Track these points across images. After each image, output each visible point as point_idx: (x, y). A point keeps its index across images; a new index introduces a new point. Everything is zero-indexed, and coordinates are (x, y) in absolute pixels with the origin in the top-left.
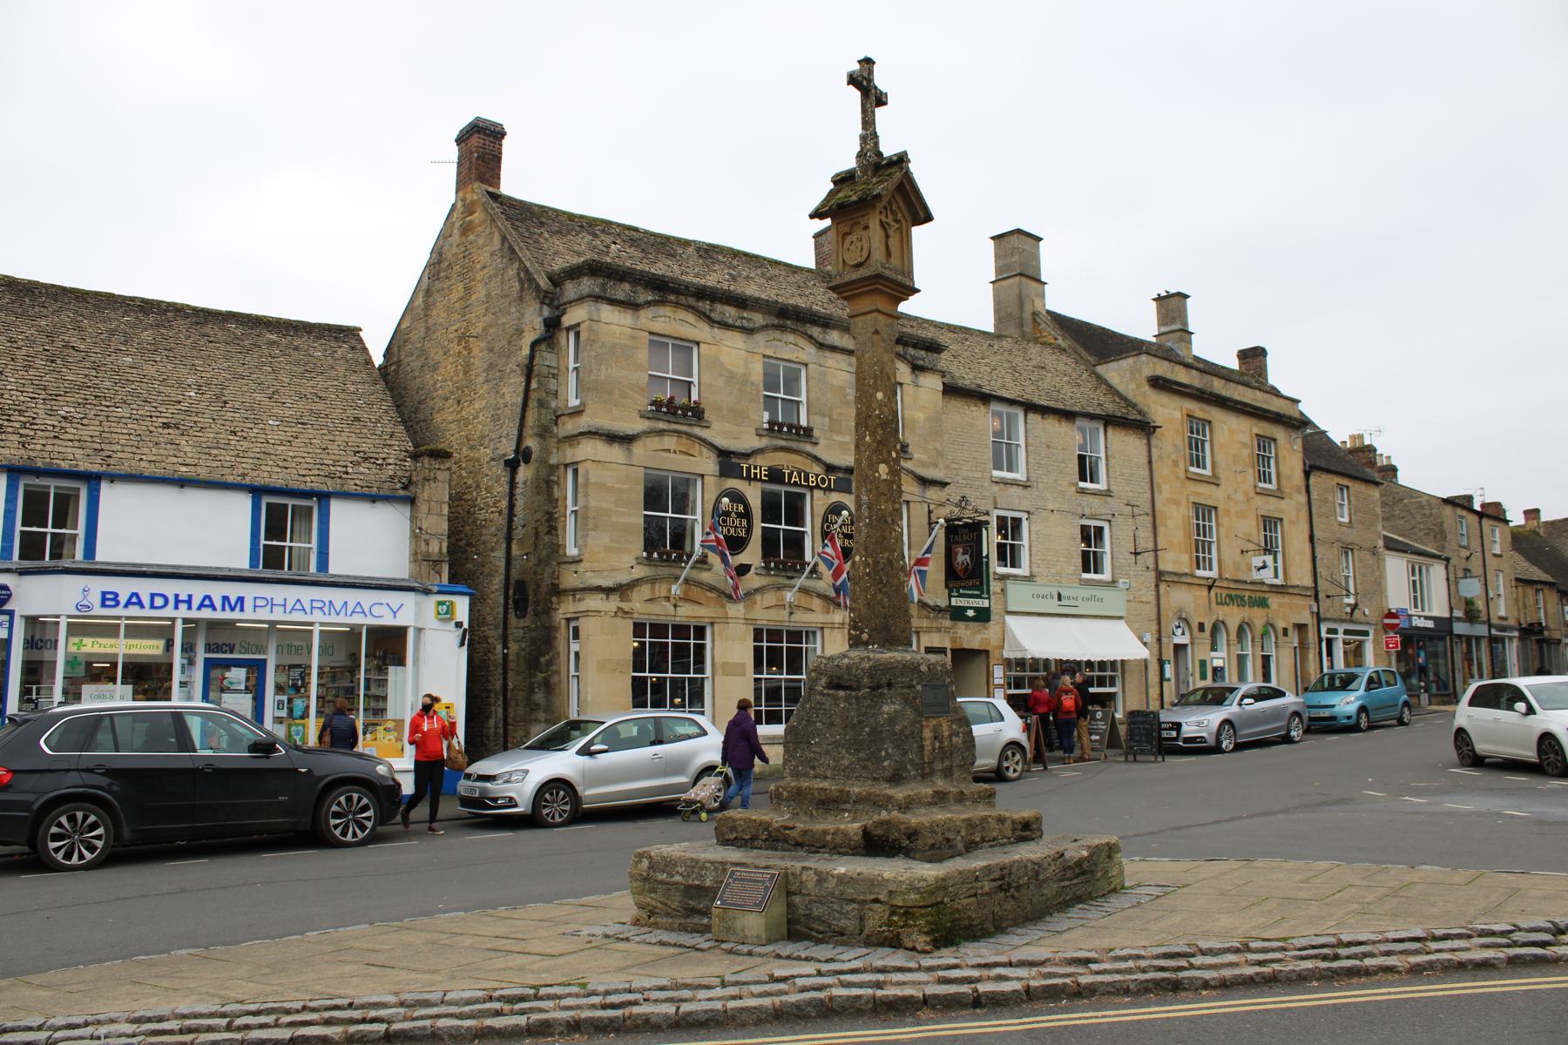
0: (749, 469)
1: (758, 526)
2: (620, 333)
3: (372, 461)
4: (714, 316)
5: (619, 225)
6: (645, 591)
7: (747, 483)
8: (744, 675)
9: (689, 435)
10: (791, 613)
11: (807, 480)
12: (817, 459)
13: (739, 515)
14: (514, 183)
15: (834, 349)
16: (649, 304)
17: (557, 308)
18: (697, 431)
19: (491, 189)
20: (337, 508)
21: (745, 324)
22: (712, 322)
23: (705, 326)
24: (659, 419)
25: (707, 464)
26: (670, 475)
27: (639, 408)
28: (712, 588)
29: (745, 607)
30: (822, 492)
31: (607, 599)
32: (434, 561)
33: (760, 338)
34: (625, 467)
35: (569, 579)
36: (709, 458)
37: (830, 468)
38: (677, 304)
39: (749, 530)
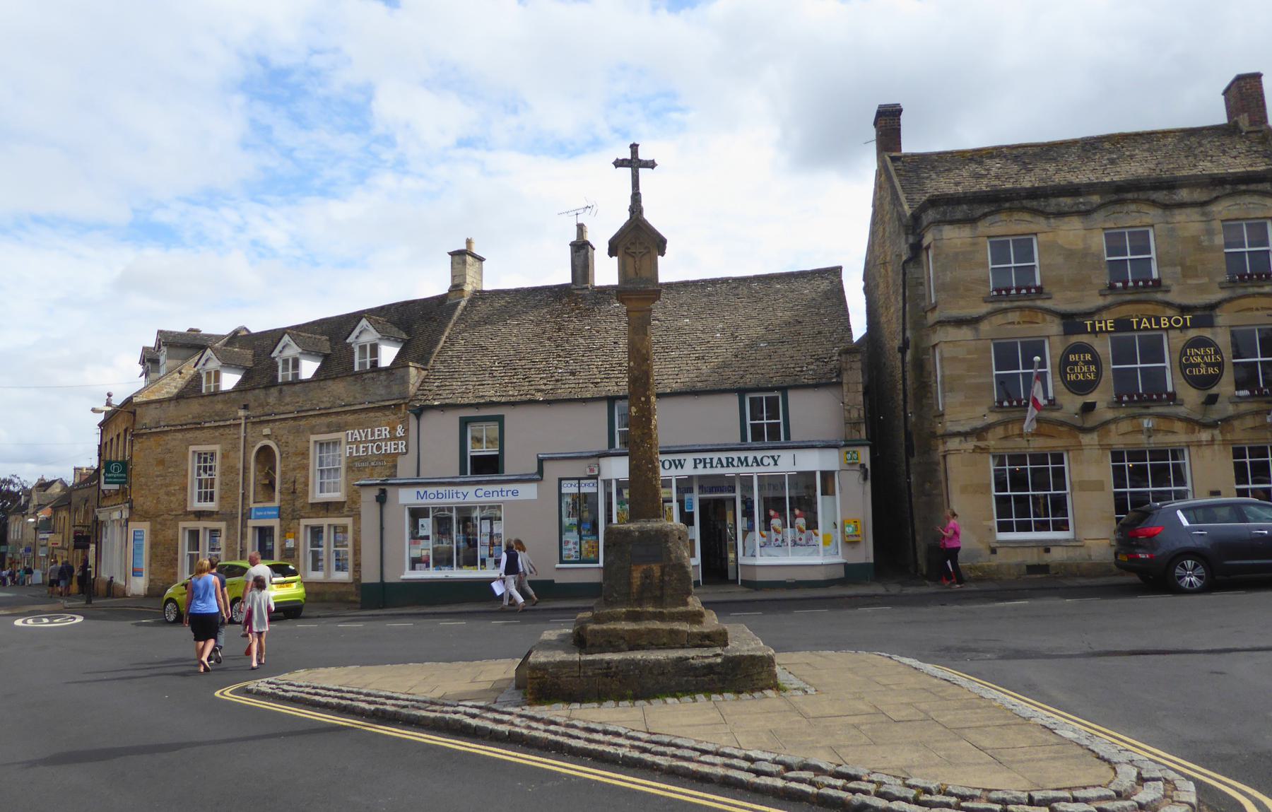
0: (1093, 326)
1: (1109, 367)
2: (961, 244)
3: (821, 360)
4: (1048, 210)
5: (1008, 147)
6: (1000, 431)
7: (1093, 336)
8: (1103, 490)
9: (1031, 308)
10: (1150, 437)
11: (1158, 322)
12: (1168, 304)
13: (1087, 363)
14: (911, 144)
15: (1182, 205)
16: (985, 215)
17: (919, 234)
18: (1039, 303)
19: (894, 154)
20: (793, 397)
21: (1083, 208)
22: (1046, 215)
23: (1042, 220)
24: (1003, 301)
25: (1054, 327)
26: (1019, 341)
27: (983, 295)
28: (1062, 423)
29: (1098, 436)
30: (1178, 331)
31: (966, 440)
32: (854, 423)
33: (1098, 217)
34: (974, 342)
35: (940, 429)
36: (1053, 322)
37: (1184, 309)
38: (1011, 210)
39: (1098, 374)
